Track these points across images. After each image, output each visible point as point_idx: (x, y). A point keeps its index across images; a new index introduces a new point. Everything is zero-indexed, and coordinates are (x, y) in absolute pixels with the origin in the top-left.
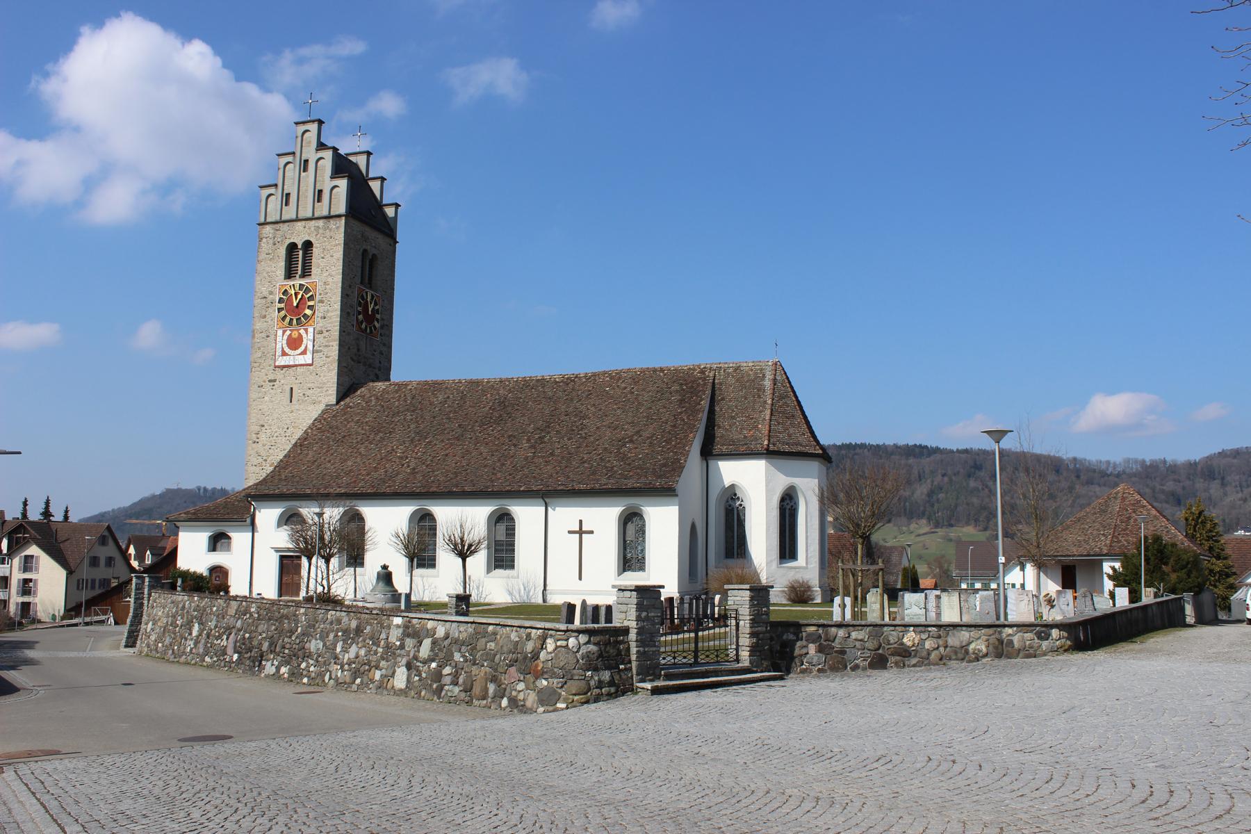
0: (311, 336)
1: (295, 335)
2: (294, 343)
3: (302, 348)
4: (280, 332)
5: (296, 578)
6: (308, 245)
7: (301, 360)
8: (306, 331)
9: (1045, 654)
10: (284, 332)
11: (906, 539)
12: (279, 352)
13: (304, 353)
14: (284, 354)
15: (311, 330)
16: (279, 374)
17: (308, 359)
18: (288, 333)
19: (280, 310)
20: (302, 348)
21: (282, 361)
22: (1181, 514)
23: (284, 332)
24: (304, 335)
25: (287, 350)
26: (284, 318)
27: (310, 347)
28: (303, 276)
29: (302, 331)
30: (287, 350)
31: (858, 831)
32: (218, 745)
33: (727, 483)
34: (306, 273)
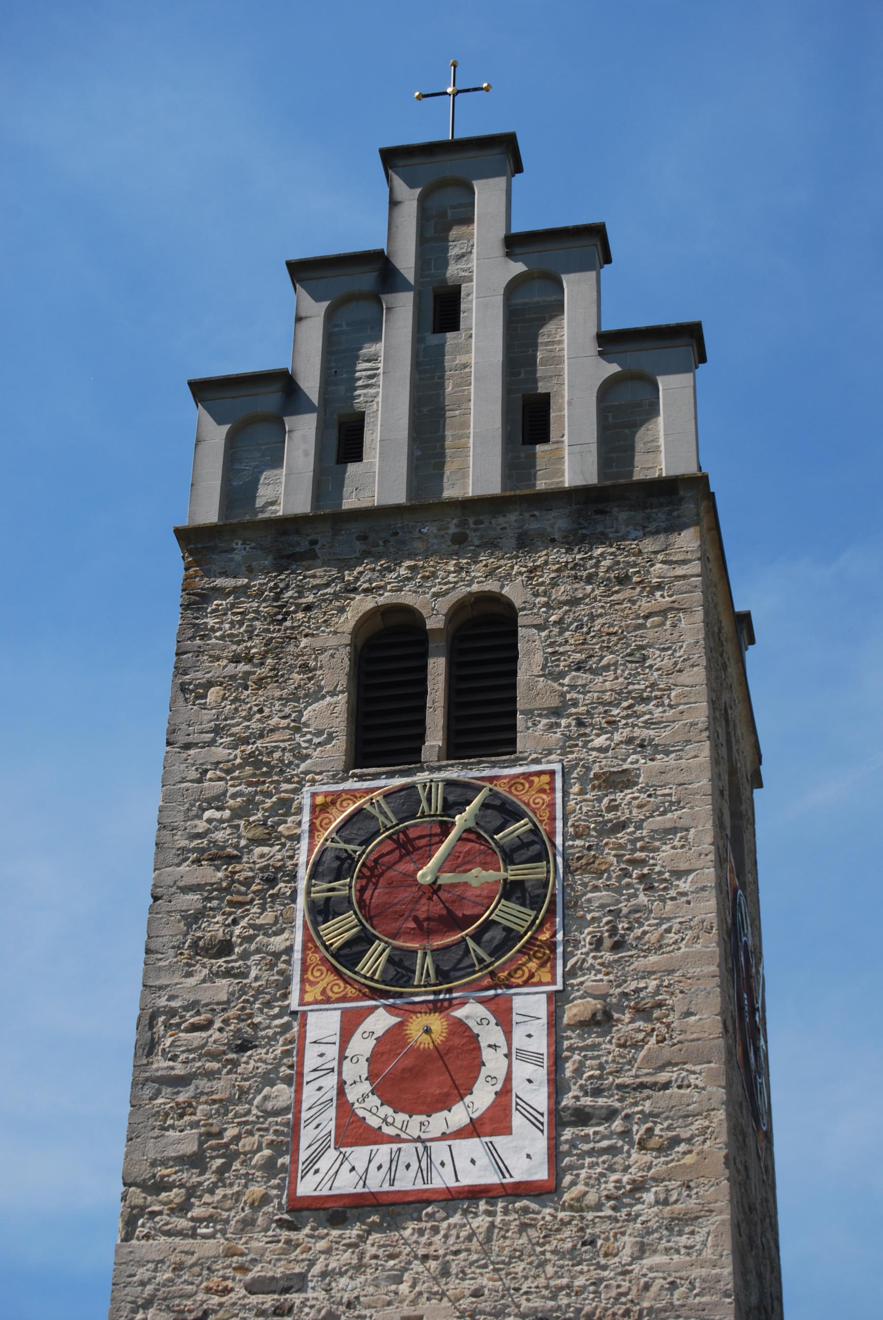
0: (532, 1035)
1: (427, 1030)
2: (422, 1078)
3: (482, 1097)
4: (324, 1024)
7: (469, 1164)
8: (504, 1018)
9: (624, 600)
10: (349, 1026)
11: (532, 837)
14: (352, 1131)
15: (530, 1005)
16: (325, 1248)
17: (525, 1154)
18: (380, 1021)
19: (322, 911)
20: (482, 1097)
21: (332, 1173)
22: (242, 1284)
23: (349, 1026)
24: (490, 1034)
25: (373, 1111)
26: (349, 955)
27: (538, 1098)
29: (472, 1012)
30: (373, 1111)
33: (542, 388)
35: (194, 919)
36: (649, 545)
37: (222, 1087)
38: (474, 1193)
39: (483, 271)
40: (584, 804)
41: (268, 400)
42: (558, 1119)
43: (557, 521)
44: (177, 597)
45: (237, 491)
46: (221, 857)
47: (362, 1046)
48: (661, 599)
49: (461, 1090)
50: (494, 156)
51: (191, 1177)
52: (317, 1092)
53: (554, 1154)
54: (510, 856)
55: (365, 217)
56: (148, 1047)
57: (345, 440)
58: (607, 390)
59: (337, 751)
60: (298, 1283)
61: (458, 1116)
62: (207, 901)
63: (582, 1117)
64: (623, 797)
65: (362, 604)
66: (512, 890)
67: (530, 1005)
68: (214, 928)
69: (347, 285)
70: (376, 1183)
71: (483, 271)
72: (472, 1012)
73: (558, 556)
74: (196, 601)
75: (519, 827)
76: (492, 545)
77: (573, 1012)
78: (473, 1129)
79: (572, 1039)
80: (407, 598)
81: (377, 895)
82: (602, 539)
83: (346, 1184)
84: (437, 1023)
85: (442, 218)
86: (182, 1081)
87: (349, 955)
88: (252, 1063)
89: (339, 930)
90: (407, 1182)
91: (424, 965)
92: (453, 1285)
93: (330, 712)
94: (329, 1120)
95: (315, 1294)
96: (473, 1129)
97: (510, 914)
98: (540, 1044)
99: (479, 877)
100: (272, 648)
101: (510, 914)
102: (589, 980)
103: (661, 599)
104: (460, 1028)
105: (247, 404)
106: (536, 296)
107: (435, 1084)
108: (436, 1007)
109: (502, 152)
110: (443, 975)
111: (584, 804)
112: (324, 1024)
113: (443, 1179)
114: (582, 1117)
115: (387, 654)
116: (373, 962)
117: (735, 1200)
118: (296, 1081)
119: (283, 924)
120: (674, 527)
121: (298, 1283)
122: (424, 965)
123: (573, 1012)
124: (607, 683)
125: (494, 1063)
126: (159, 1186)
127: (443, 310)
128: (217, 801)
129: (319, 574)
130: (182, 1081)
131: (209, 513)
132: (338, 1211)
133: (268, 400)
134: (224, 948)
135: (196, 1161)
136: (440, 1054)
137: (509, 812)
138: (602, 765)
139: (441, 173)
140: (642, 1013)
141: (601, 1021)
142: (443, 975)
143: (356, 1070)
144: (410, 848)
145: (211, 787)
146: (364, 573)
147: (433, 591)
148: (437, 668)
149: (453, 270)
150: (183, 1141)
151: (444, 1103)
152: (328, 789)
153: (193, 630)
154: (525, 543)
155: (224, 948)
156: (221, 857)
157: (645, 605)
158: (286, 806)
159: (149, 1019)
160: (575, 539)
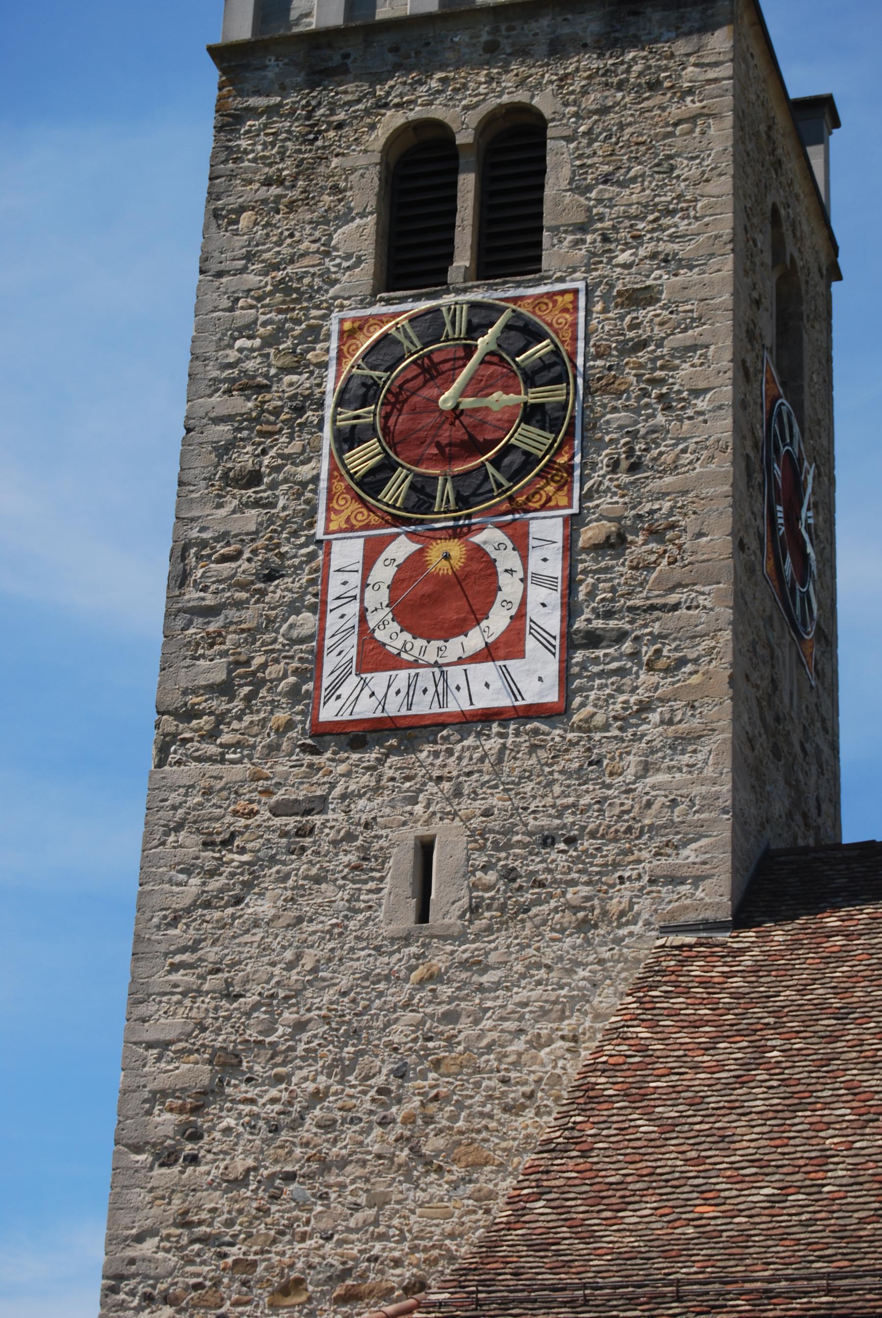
0: (548, 560)
2: (441, 603)
3: (497, 622)
4: (347, 552)
5: (548, 407)
6: (517, 140)
7: (484, 687)
10: (372, 553)
12: (340, 653)
13: (507, 647)
14: (373, 657)
15: (546, 529)
16: (345, 770)
17: (536, 676)
18: (402, 548)
20: (497, 622)
21: (353, 699)
23: (372, 553)
24: (507, 560)
25: (391, 635)
27: (549, 619)
28: (487, 268)
29: (490, 537)
30: (391, 635)
31: (736, 1315)
32: (816, 811)
34: (512, 247)
35: (224, 450)
36: (681, 47)
37: (250, 616)
42: (570, 641)
46: (251, 387)
47: (383, 573)
48: (692, 105)
49: (478, 615)
51: (220, 704)
52: (340, 619)
53: (565, 677)
56: (180, 579)
59: (364, 275)
60: (319, 805)
61: (474, 640)
63: (593, 639)
64: (645, 314)
65: (393, 120)
66: (532, 414)
67: (546, 529)
68: (244, 459)
70: (395, 708)
72: (490, 537)
73: (590, 62)
74: (229, 122)
75: (541, 349)
76: (523, 52)
77: (589, 534)
78: (488, 653)
79: (587, 562)
80: (437, 112)
81: (401, 422)
82: (635, 42)
83: (366, 709)
84: (456, 549)
86: (211, 612)
87: (372, 482)
88: (280, 591)
90: (424, 706)
91: (445, 490)
92: (465, 806)
93: (359, 235)
95: (335, 815)
96: (488, 653)
97: (530, 438)
98: (555, 568)
99: (499, 400)
100: (304, 170)
101: (530, 438)
102: (604, 503)
103: (692, 105)
104: (478, 553)
107: (452, 610)
108: (456, 533)
110: (463, 501)
111: (607, 322)
112: (347, 552)
113: (458, 703)
114: (593, 639)
115: (418, 167)
116: (396, 490)
118: (320, 609)
119: (310, 454)
120: (708, 27)
121: (319, 805)
122: (445, 490)
123: (589, 534)
124: (634, 195)
125: (510, 587)
128: (248, 330)
129: (351, 89)
130: (211, 612)
135: (225, 689)
137: (534, 334)
140: (656, 535)
141: (615, 544)
142: (463, 501)
144: (434, 372)
145: (243, 316)
146: (394, 87)
148: (467, 184)
150: (214, 670)
151: (460, 628)
152: (360, 316)
153: (225, 152)
154: (557, 49)
155: (253, 478)
156: (251, 387)
157: (675, 112)
158: (315, 333)
159: (181, 552)
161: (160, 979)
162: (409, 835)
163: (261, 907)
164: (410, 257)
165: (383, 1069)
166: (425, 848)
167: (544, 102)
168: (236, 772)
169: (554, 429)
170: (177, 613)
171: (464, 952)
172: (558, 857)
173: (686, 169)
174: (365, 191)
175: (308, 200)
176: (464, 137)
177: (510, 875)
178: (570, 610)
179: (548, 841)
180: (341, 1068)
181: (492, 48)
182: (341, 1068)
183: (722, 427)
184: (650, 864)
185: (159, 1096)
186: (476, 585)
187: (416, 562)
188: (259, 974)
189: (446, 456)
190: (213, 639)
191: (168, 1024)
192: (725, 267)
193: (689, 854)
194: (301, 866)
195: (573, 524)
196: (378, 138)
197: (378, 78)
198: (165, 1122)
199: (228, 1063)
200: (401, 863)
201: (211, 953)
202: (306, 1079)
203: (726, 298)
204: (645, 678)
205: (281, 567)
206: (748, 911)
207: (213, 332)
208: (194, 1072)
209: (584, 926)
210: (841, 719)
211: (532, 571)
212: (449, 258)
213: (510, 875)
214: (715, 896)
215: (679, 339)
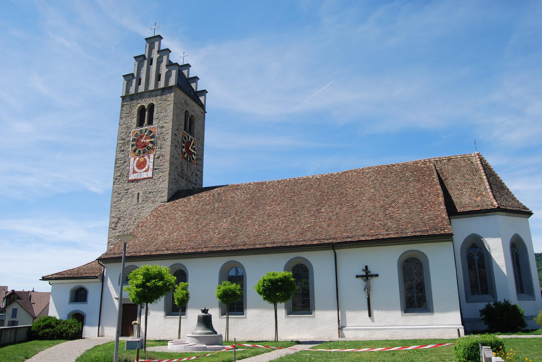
1: (142, 160)
2: (141, 165)
3: (146, 167)
4: (132, 159)
6: (152, 106)
7: (145, 175)
8: (149, 157)
10: (135, 159)
12: (132, 171)
14: (134, 172)
15: (152, 156)
16: (131, 185)
18: (137, 159)
21: (132, 177)
23: (135, 159)
24: (148, 160)
25: (136, 169)
26: (135, 151)
27: (151, 167)
29: (146, 157)
30: (136, 169)
34: (150, 122)
35: (121, 147)
36: (169, 95)
37: (122, 167)
38: (145, 178)
39: (155, 56)
40: (159, 130)
41: (131, 77)
42: (154, 169)
43: (159, 92)
44: (120, 106)
45: (127, 91)
46: (124, 140)
47: (136, 162)
48: (169, 103)
49: (145, 167)
50: (157, 38)
51: (119, 178)
52: (131, 167)
53: (153, 174)
54: (151, 138)
55: (143, 50)
56: (116, 163)
57: (139, 83)
58: (167, 73)
59: (135, 126)
60: (128, 189)
61: (144, 170)
62: (122, 142)
63: (156, 169)
64: (163, 129)
65: (139, 105)
66: (151, 142)
67: (152, 156)
68: (122, 148)
69: (140, 59)
70: (136, 178)
71: (155, 56)
72: (146, 157)
73: (159, 97)
74: (123, 106)
75: (152, 134)
76: (153, 96)
77: (156, 157)
78: (145, 171)
79: (156, 160)
80: (143, 104)
81: (138, 143)
82: (164, 95)
83: (133, 178)
84: (143, 159)
85: (151, 48)
86: (119, 167)
87: (135, 151)
88: (126, 164)
89: (134, 147)
90: (139, 178)
91: (142, 152)
92: (143, 189)
93: (135, 120)
94: (132, 171)
95: (130, 190)
96: (145, 171)
97: (150, 145)
98: (152, 161)
99: (148, 140)
100: (130, 112)
101: (150, 145)
102: (157, 153)
103: (169, 103)
104: (145, 159)
105: (128, 78)
106: (160, 60)
107: (142, 166)
108: (143, 157)
109: (159, 37)
110: (144, 153)
111: (159, 130)
112: (132, 159)
113: (142, 177)
114: (156, 169)
115: (142, 110)
116: (137, 152)
117: (97, 354)
118: (129, 166)
119: (129, 148)
120: (171, 93)
121: (128, 189)
122: (142, 152)
123: (156, 157)
124: (163, 114)
125: (148, 163)
126: (117, 179)
127: (151, 62)
128: (123, 132)
129: (135, 101)
130: (119, 167)
131: (124, 95)
132: (133, 181)
133: (131, 77)
134: (123, 151)
135: (120, 176)
136: (143, 162)
137: (151, 132)
138: (161, 125)
139: (152, 41)
140: (162, 156)
141: (158, 158)
142: (144, 153)
143: (135, 165)
144: (141, 137)
145: (123, 131)
146: (139, 101)
147: (146, 102)
148: (147, 113)
149: (152, 56)
150: (119, 174)
151: (143, 168)
152: (135, 129)
153: (122, 110)
154: (156, 96)
155: (123, 151)
156: (124, 140)
157: (168, 103)
158: (130, 133)
159: (116, 160)
160: (162, 95)
161: (113, 210)
162: (137, 193)
163: (123, 201)
164: (140, 123)
165: (134, 218)
166: (139, 194)
167: (154, 103)
168: (120, 186)
169: (168, 290)
170: (116, 167)
171: (142, 206)
172: (151, 195)
173: (168, 111)
174: (136, 115)
175: (130, 116)
176: (146, 107)
177: (146, 197)
178: (154, 166)
179: (150, 193)
180: (130, 219)
181: (149, 96)
182: (130, 219)
183: (170, 143)
184: (160, 195)
185: (113, 222)
186: (145, 162)
187: (139, 160)
188: (123, 209)
189: (142, 148)
190: (119, 170)
191: (114, 215)
192: (171, 124)
193: (164, 194)
194: (127, 196)
195: (154, 155)
196: (137, 108)
197: (138, 100)
198: (113, 225)
199: (119, 219)
200: (136, 195)
201: (118, 206)
202: (127, 220)
203: (171, 127)
204: (161, 173)
205: (126, 161)
206: (169, 201)
207: (120, 132)
208: (116, 220)
209: (153, 202)
210: (78, 340)
211: (150, 163)
212: (144, 122)
213: (146, 197)
214: (166, 199)
215: (166, 132)
